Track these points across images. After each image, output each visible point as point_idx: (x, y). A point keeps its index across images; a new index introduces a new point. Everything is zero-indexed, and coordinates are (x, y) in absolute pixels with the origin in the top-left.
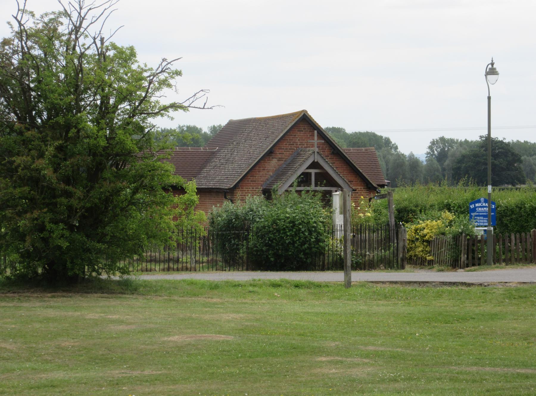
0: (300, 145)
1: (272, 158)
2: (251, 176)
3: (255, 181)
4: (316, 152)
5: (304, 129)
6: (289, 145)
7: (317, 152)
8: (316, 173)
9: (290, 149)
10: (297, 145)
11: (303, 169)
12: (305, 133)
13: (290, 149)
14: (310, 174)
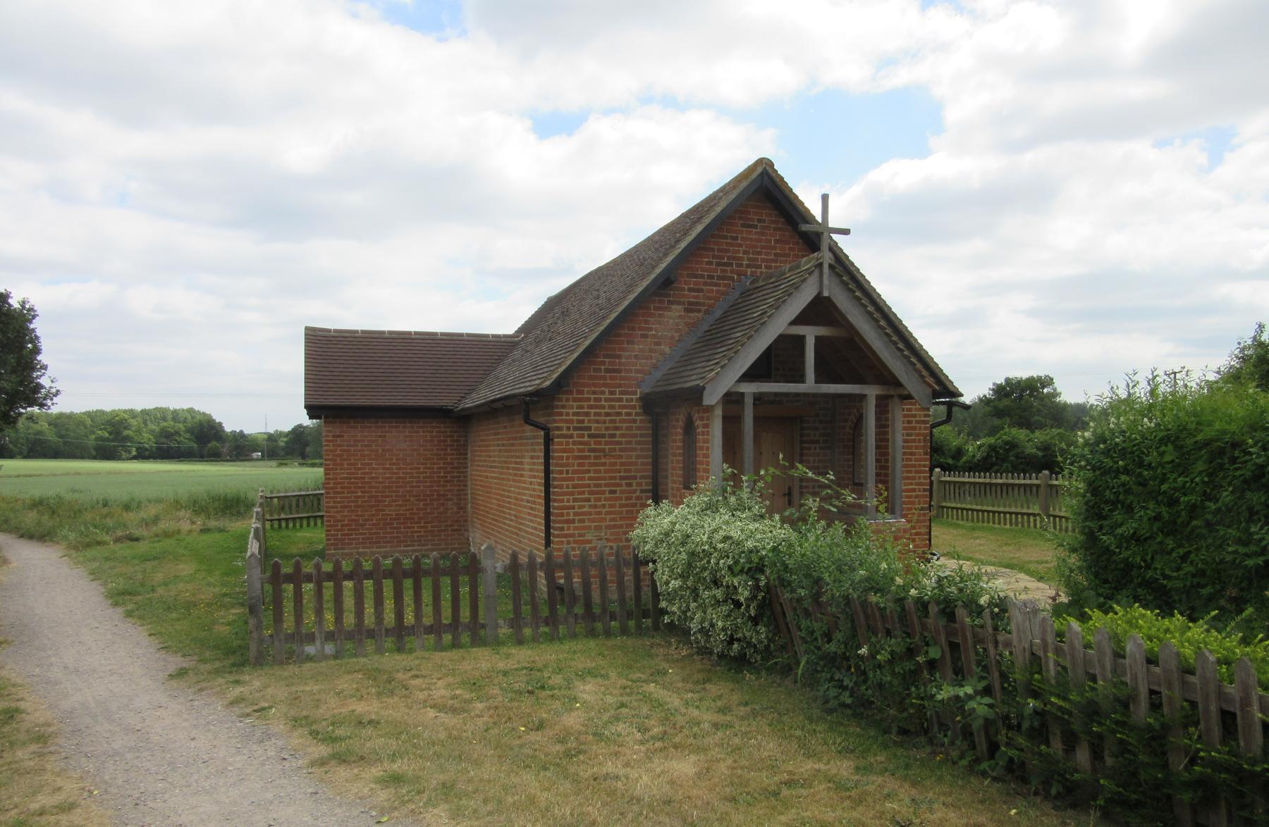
0: (748, 266)
1: (670, 302)
2: (605, 356)
3: (618, 371)
4: (826, 266)
5: (759, 221)
6: (718, 264)
7: (831, 266)
8: (801, 379)
9: (719, 278)
10: (741, 265)
11: (779, 325)
12: (763, 234)
14: (801, 340)
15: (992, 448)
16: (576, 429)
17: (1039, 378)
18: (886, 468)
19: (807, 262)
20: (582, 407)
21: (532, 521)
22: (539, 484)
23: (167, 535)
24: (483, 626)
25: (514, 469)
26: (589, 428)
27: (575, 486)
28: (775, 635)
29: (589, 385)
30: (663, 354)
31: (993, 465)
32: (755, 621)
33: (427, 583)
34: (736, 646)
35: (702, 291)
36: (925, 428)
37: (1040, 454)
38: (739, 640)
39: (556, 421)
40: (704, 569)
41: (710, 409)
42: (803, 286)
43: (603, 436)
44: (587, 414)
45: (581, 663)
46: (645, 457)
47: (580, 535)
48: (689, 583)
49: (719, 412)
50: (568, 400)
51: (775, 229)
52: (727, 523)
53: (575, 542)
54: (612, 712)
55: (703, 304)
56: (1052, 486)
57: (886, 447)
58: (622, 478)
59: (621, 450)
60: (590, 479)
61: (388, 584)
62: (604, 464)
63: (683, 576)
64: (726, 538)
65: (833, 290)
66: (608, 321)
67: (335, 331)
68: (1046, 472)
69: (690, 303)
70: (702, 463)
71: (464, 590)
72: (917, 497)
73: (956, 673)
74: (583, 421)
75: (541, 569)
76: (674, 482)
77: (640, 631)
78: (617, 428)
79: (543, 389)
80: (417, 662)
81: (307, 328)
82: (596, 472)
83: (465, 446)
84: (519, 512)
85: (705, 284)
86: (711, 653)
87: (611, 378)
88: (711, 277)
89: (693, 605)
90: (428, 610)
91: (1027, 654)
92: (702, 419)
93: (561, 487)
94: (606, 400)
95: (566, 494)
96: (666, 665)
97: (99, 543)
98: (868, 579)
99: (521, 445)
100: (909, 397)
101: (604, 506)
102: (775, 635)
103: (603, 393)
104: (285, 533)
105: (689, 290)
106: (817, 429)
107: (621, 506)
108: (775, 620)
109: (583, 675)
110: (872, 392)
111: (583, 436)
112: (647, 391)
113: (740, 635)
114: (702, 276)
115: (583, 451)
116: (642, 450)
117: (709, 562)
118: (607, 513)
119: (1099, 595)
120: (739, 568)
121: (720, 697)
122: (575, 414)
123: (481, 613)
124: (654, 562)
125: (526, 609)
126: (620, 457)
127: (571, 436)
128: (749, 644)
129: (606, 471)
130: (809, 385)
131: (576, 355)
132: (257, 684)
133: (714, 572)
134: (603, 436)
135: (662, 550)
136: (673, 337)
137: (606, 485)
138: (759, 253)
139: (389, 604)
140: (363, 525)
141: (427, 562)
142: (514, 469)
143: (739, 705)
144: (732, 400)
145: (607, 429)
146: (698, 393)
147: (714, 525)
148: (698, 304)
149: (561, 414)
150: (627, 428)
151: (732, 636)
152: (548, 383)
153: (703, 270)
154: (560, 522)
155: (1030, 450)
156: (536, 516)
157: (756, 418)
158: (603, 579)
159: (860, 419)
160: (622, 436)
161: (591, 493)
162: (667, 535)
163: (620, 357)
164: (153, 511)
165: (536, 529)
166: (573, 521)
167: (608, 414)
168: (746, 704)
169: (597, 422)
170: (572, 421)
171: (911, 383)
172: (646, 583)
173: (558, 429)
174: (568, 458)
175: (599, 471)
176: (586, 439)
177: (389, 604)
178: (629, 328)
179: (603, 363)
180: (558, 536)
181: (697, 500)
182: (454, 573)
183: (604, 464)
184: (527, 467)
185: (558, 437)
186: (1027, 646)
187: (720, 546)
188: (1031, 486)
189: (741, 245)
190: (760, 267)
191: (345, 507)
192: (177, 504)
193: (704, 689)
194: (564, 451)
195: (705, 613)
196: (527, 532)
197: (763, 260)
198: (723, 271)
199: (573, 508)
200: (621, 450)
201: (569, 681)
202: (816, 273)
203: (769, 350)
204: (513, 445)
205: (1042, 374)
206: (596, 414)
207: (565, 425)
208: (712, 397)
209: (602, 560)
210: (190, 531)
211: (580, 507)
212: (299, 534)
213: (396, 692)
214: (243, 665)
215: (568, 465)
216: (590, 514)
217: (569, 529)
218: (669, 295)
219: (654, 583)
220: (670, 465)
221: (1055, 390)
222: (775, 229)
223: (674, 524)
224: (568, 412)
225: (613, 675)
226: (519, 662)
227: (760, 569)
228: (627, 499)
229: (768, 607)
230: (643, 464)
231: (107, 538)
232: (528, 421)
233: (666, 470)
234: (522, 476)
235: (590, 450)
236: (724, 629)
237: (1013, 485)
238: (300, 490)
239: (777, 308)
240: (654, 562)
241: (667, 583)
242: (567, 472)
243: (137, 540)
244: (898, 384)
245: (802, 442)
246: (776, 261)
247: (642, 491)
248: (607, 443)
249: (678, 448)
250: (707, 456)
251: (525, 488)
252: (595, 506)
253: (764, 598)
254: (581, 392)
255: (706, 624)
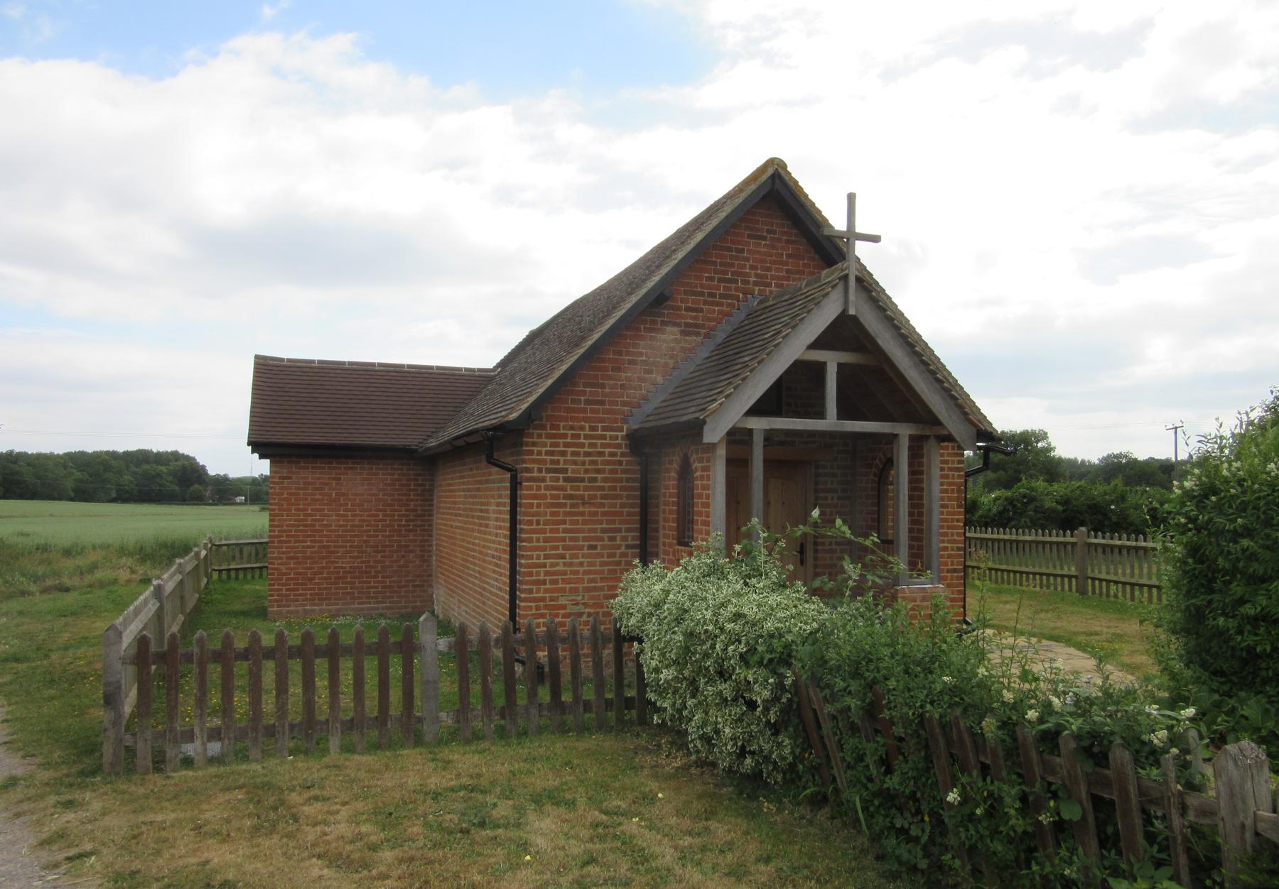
0: (756, 284)
1: (663, 323)
3: (602, 403)
5: (769, 231)
6: (720, 280)
8: (821, 415)
9: (722, 296)
10: (747, 282)
12: (773, 247)
13: (722, 296)
14: (820, 368)
15: (1010, 501)
16: (549, 471)
17: (1033, 433)
18: (921, 523)
19: (828, 275)
20: (557, 445)
21: (496, 580)
22: (505, 537)
23: (101, 585)
24: (420, 720)
25: (479, 518)
26: (565, 471)
27: (546, 540)
28: (804, 750)
29: (566, 419)
30: (654, 383)
31: (1010, 519)
32: (776, 729)
33: (346, 666)
34: (748, 761)
35: (701, 310)
36: (959, 477)
37: (1060, 508)
38: (752, 753)
39: (524, 461)
40: (706, 655)
41: (712, 447)
42: (826, 300)
43: (582, 480)
44: (563, 454)
45: (544, 779)
46: (632, 506)
47: (552, 599)
48: (686, 673)
49: (722, 452)
50: (540, 436)
51: (788, 242)
52: (738, 595)
53: (546, 607)
54: (576, 873)
55: (703, 326)
56: (1090, 545)
57: (921, 498)
58: (604, 531)
59: (603, 497)
60: (566, 531)
61: (296, 666)
62: (583, 514)
63: (679, 663)
64: (737, 616)
65: (859, 307)
66: (590, 343)
67: (289, 360)
68: (1083, 529)
69: (687, 325)
70: (700, 514)
71: (396, 670)
72: (949, 556)
73: (1102, 844)
74: (558, 462)
75: (496, 645)
76: (665, 536)
77: (622, 726)
78: (598, 471)
79: (507, 422)
80: (324, 773)
81: (257, 357)
82: (572, 523)
83: (431, 491)
84: (485, 568)
85: (705, 303)
86: (714, 765)
87: (593, 411)
88: (712, 295)
89: (690, 702)
90: (346, 701)
91: (1249, 835)
92: (701, 460)
93: (530, 540)
94: (586, 437)
95: (536, 549)
96: (654, 785)
97: (23, 593)
98: (953, 690)
99: (487, 489)
100: (949, 438)
101: (581, 564)
102: (804, 750)
103: (582, 428)
104: (233, 584)
105: (687, 309)
106: (834, 475)
107: (603, 564)
108: (805, 730)
109: (540, 800)
110: (904, 431)
111: (558, 479)
112: (635, 427)
113: (754, 747)
114: (702, 294)
115: (557, 497)
116: (628, 497)
117: (713, 647)
118: (585, 572)
119: (1213, 691)
120: (756, 658)
121: (730, 845)
122: (548, 453)
123: (418, 702)
124: (641, 641)
125: (476, 701)
126: (602, 505)
127: (543, 480)
128: (767, 759)
129: (585, 522)
130: (830, 422)
131: (550, 382)
132: (97, 806)
133: (720, 662)
134: (582, 480)
135: (651, 627)
136: (666, 364)
137: (585, 539)
138: (769, 269)
139: (295, 689)
140: (311, 579)
141: (346, 639)
142: (479, 518)
143: (758, 860)
144: (739, 438)
145: (587, 471)
146: (696, 428)
147: (721, 597)
148: (696, 326)
149: (531, 453)
150: (612, 471)
151: (743, 748)
152: (515, 415)
153: (702, 286)
154: (527, 583)
155: (1049, 504)
156: (501, 575)
157: (766, 462)
158: (576, 659)
159: (890, 463)
160: (605, 480)
161: (565, 548)
162: (658, 606)
163: (603, 386)
164: (93, 557)
165: (500, 589)
166: (544, 582)
167: (587, 454)
168: (767, 860)
169: (575, 463)
170: (544, 462)
171: (952, 423)
172: (629, 669)
173: (528, 470)
174: (539, 506)
175: (577, 522)
176: (561, 483)
177: (295, 689)
178: (615, 353)
179: (584, 393)
180: (526, 600)
181: (697, 562)
182: (382, 651)
183: (583, 514)
184: (492, 515)
185: (529, 480)
186: (1249, 822)
187: (729, 626)
188: (1065, 544)
189: (748, 260)
190: (769, 285)
191: (292, 558)
192: (123, 551)
193: (707, 829)
194: (535, 497)
195: (707, 714)
196: (491, 593)
197: (773, 278)
198: (725, 289)
199: (544, 566)
200: (603, 497)
201: (520, 811)
202: (840, 288)
203: (779, 383)
204: (478, 490)
205: (1036, 428)
206: (573, 454)
207: (536, 466)
208: (715, 433)
209: (575, 635)
210: (129, 581)
211: (552, 565)
212: (247, 587)
213: (281, 826)
214: (93, 773)
215: (537, 514)
216: (565, 573)
217: (538, 591)
218: (663, 315)
219: (639, 666)
220: (662, 515)
221: (1049, 444)
222: (788, 242)
223: (667, 593)
224: (540, 451)
225: (582, 802)
226: (458, 775)
227: (785, 658)
228: (610, 556)
229: (794, 714)
230: (629, 514)
231: (33, 588)
232: (492, 462)
233: (657, 522)
234: (487, 526)
235: (566, 497)
236: (734, 739)
237: (1044, 543)
238: (253, 537)
239: (794, 327)
240: (641, 641)
241: (657, 670)
242: (538, 523)
243: (67, 590)
244: (937, 422)
245: (816, 491)
246: (788, 279)
247: (628, 547)
248: (586, 489)
249: (671, 495)
250: (707, 505)
251: (490, 541)
252: (571, 564)
253: (789, 700)
254: (557, 428)
255: (709, 729)
